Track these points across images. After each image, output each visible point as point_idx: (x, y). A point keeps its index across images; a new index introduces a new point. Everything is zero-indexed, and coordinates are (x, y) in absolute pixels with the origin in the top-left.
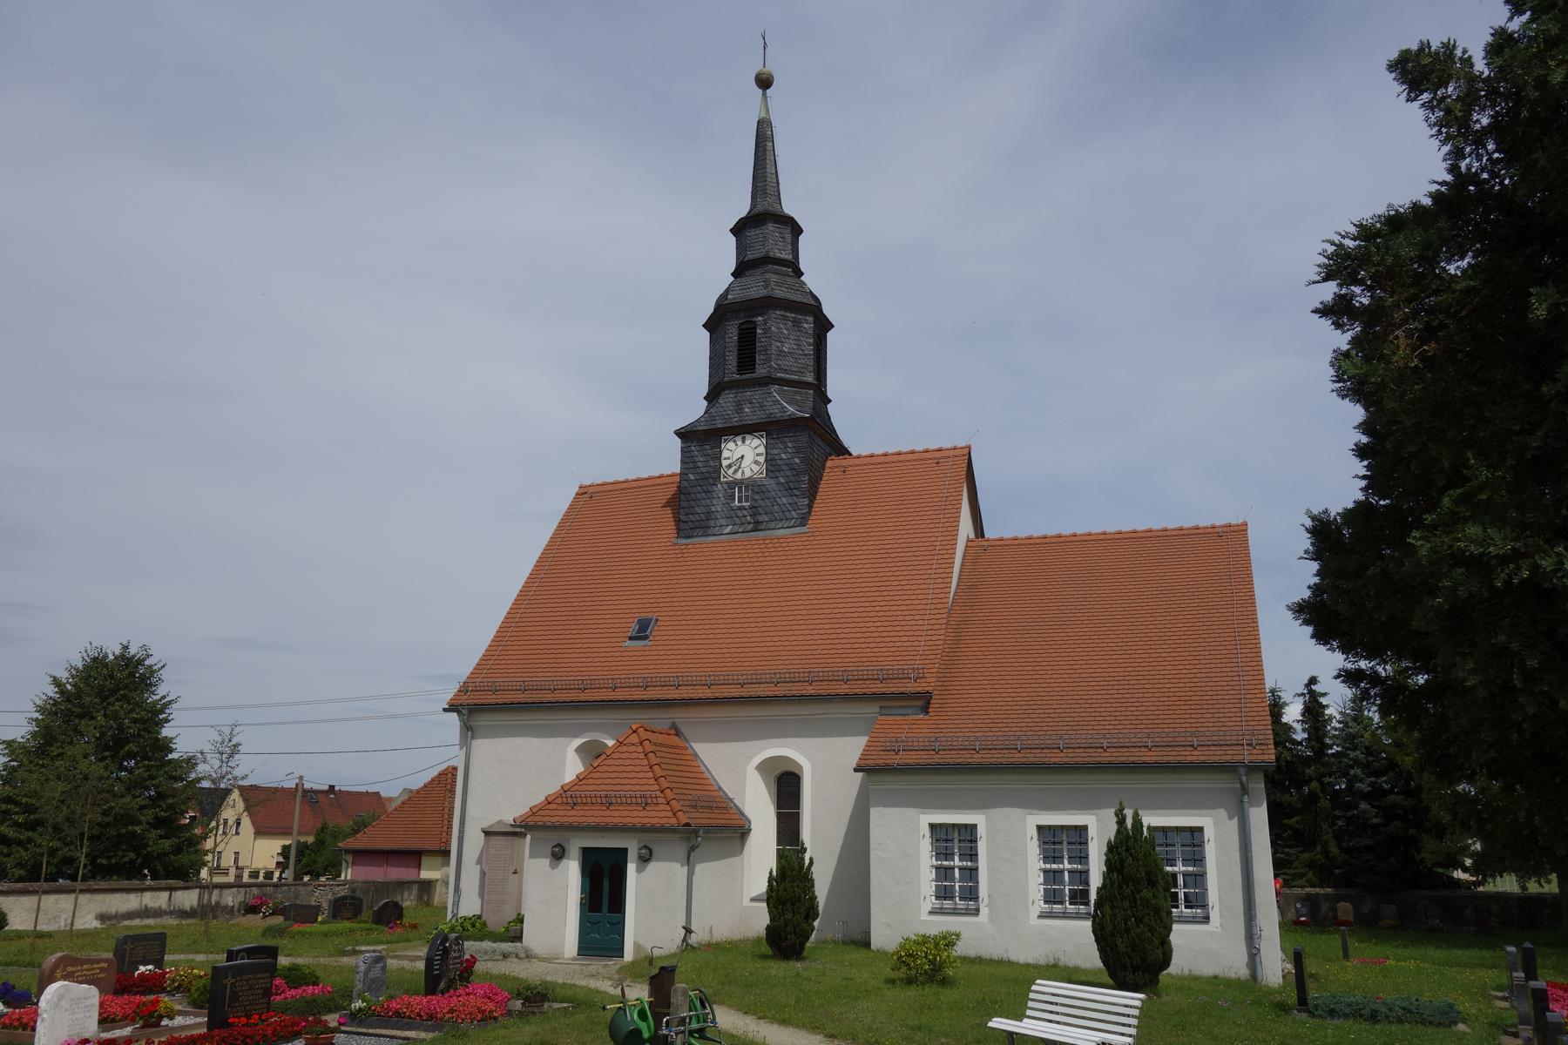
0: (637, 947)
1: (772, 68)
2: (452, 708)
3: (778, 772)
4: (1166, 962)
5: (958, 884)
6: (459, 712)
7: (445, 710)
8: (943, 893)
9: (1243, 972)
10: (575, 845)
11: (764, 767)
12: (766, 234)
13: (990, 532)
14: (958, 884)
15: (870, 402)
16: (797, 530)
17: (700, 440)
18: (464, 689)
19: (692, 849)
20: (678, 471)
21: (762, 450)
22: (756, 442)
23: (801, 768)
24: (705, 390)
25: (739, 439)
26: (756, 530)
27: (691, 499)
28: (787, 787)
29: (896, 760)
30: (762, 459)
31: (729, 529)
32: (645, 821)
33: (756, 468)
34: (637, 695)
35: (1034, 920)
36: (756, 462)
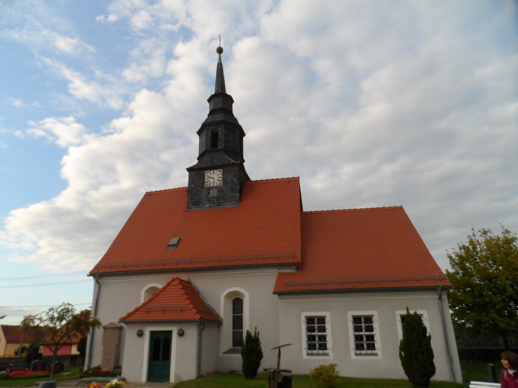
0: (176, 375)
1: (222, 46)
2: (92, 274)
3: (233, 298)
4: (433, 372)
5: (317, 342)
6: (94, 277)
7: (88, 276)
8: (311, 347)
9: (276, 367)
10: (147, 331)
11: (228, 295)
12: (221, 102)
13: (304, 211)
14: (317, 342)
15: (259, 165)
16: (235, 205)
17: (196, 172)
18: (97, 267)
19: (203, 329)
20: (186, 185)
21: (221, 176)
22: (219, 173)
23: (243, 295)
24: (197, 156)
25: (212, 172)
26: (219, 205)
27: (196, 190)
28: (237, 303)
29: (291, 289)
30: (221, 179)
31: (208, 205)
32: (181, 318)
33: (218, 182)
34: (173, 267)
35: (353, 356)
36: (219, 180)
